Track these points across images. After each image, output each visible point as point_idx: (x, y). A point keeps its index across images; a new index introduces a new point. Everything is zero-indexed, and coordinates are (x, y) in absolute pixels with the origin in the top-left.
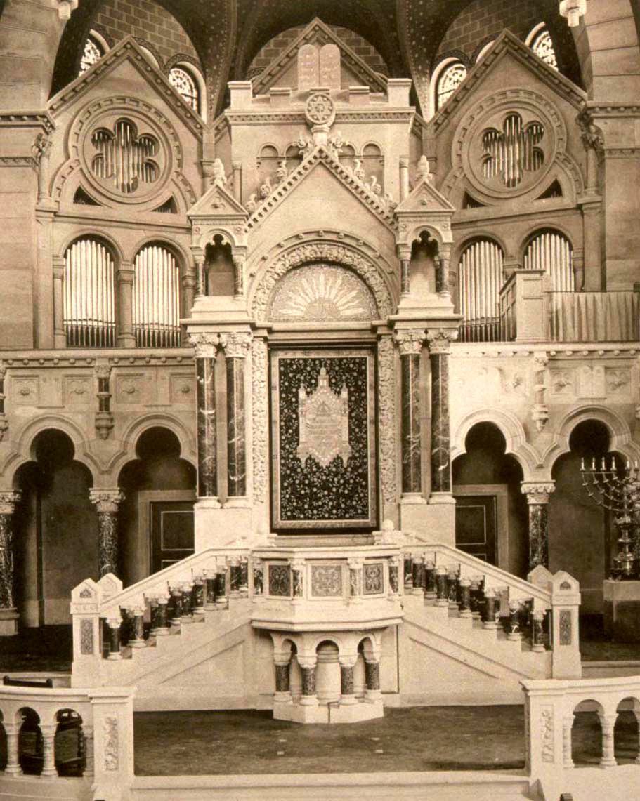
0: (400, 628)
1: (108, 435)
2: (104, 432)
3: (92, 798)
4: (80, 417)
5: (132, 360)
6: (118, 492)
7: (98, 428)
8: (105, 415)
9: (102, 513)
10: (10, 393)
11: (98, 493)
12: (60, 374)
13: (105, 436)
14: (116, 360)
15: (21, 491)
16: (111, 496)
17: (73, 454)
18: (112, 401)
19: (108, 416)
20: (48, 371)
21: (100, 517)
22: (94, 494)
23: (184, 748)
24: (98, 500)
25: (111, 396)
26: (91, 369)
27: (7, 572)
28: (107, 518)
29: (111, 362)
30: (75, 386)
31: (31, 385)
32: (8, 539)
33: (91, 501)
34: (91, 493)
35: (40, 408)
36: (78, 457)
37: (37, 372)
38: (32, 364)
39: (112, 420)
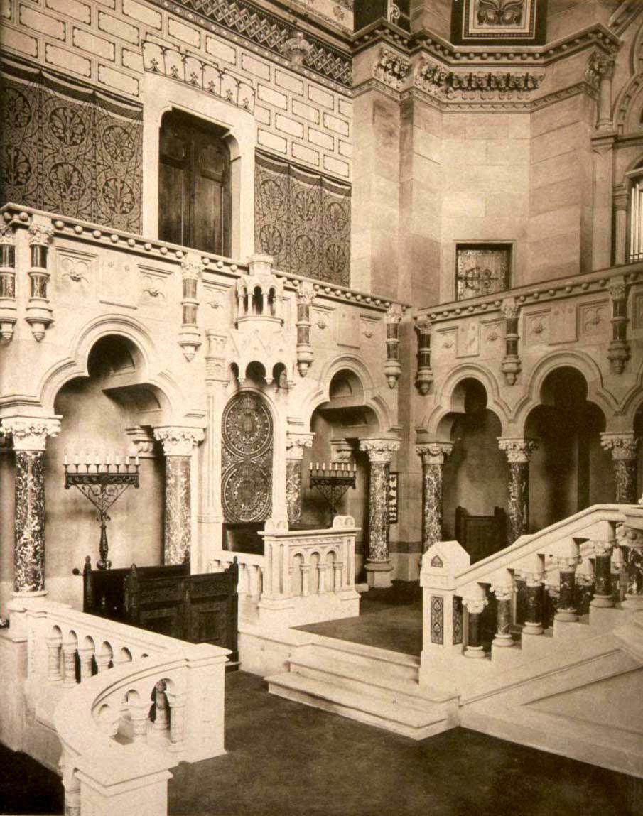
0: (456, 575)
1: (515, 380)
2: (510, 377)
3: (640, 779)
4: (594, 349)
5: (584, 286)
6: (632, 436)
7: (506, 373)
8: (511, 359)
9: (616, 462)
10: (524, 333)
11: (610, 437)
12: (572, 304)
13: (511, 382)
14: (522, 298)
15: (453, 442)
16: (624, 441)
17: (586, 396)
18: (520, 342)
19: (515, 360)
20: (562, 303)
21: (615, 467)
22: (606, 439)
23: (104, 603)
24: (610, 446)
25: (518, 338)
26: (606, 293)
27: (518, 524)
28: (622, 467)
29: (518, 300)
30: (591, 315)
31: (545, 321)
32: (521, 490)
33: (603, 447)
34: (603, 438)
35: (550, 345)
36: (590, 397)
37: (551, 305)
38: (542, 297)
39: (518, 364)
